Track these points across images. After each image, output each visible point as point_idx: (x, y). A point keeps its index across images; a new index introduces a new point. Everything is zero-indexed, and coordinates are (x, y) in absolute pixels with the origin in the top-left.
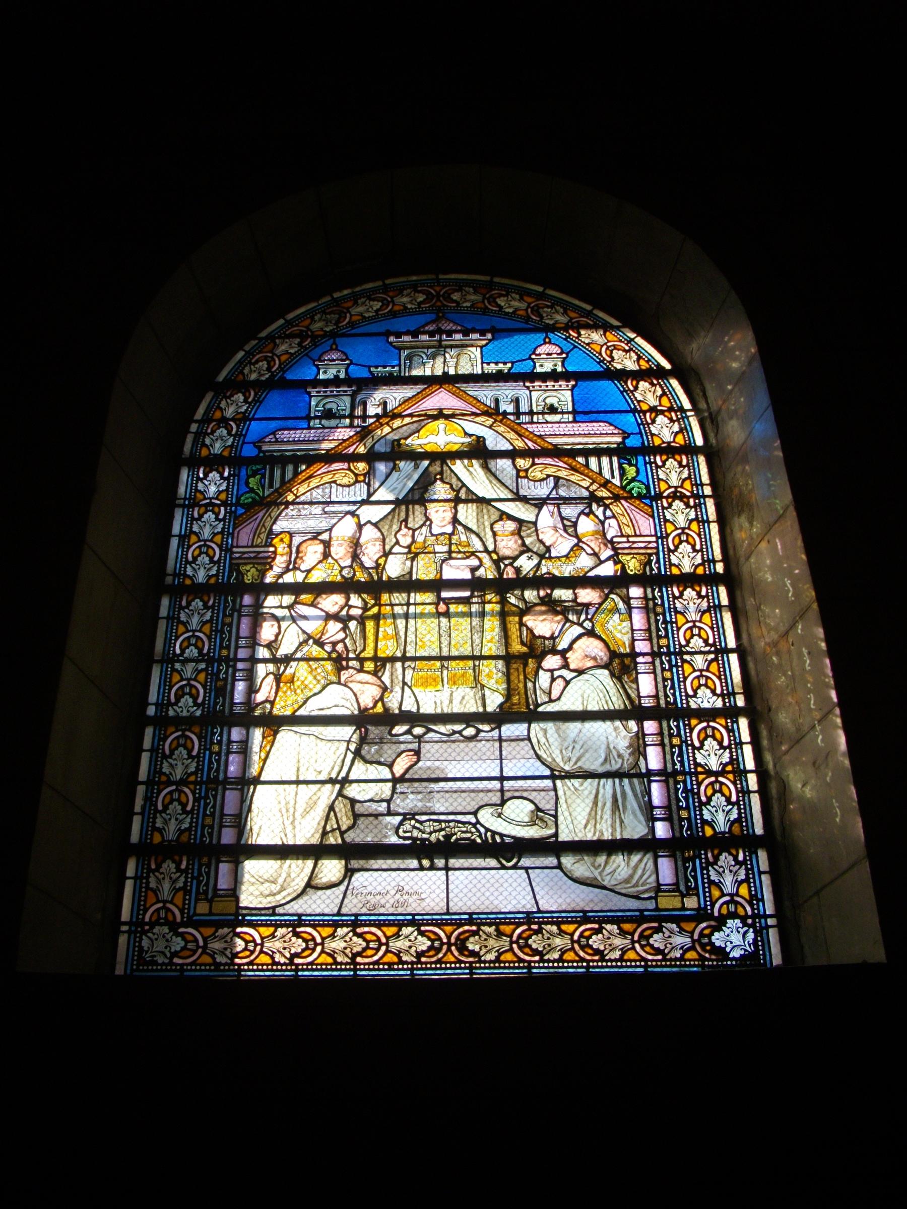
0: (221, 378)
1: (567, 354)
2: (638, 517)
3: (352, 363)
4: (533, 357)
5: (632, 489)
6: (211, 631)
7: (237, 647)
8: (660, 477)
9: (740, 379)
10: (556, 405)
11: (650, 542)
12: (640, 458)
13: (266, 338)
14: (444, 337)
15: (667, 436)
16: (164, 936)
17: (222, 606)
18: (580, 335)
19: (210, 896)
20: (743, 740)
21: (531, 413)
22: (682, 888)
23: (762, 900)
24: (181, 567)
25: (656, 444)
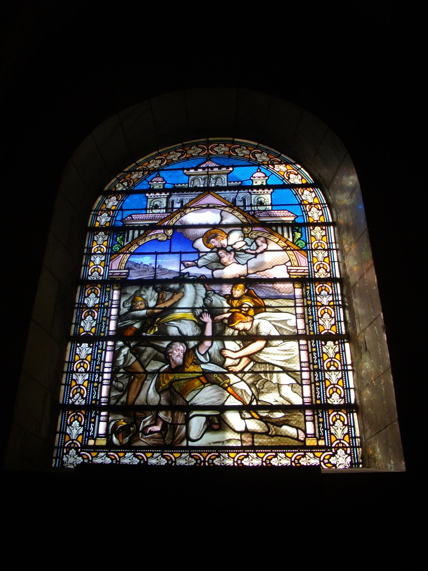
0: (106, 188)
1: (268, 177)
2: (300, 257)
3: (166, 183)
4: (252, 178)
5: (298, 244)
6: (91, 359)
7: (104, 367)
8: (324, 351)
9: (352, 190)
10: (263, 202)
11: (305, 270)
12: (303, 228)
13: (127, 172)
14: (210, 170)
15: (316, 218)
16: (73, 457)
17: (104, 297)
18: (274, 167)
19: (95, 437)
20: (351, 387)
21: (251, 205)
22: (317, 436)
23: (354, 426)
24: (66, 400)
25: (311, 221)
